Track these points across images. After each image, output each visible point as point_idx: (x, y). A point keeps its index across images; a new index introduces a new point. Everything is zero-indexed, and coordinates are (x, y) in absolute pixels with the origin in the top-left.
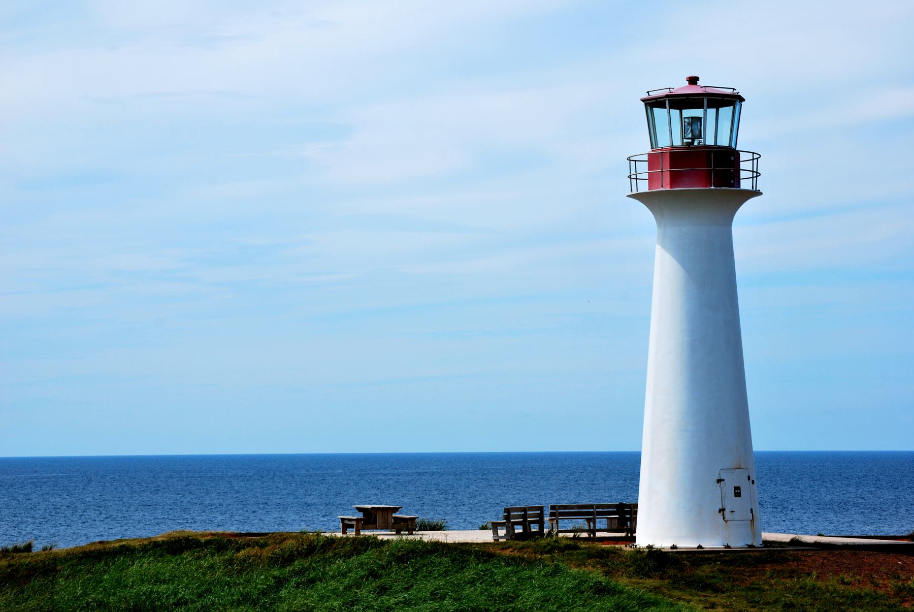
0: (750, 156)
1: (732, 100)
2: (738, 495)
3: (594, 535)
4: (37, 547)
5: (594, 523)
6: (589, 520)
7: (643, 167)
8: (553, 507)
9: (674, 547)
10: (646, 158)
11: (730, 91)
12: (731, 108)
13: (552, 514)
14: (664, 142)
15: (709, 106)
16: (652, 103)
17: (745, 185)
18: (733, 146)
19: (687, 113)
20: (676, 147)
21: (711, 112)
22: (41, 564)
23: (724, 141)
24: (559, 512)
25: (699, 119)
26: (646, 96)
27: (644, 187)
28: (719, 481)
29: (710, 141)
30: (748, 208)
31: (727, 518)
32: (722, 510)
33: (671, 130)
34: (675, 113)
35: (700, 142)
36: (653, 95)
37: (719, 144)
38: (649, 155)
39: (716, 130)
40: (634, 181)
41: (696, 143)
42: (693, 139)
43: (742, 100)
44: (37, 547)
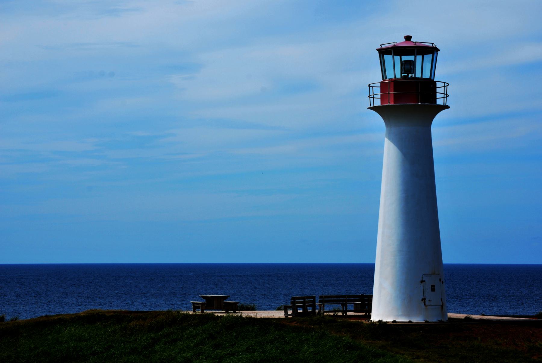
0: (442, 85)
1: (433, 50)
3: (346, 314)
6: (343, 305)
7: (378, 91)
8: (321, 297)
10: (379, 85)
13: (320, 301)
14: (390, 75)
16: (383, 52)
17: (440, 102)
18: (432, 78)
19: (405, 58)
20: (390, 82)
21: (419, 58)
27: (378, 103)
29: (418, 75)
39: (422, 69)
43: (439, 50)
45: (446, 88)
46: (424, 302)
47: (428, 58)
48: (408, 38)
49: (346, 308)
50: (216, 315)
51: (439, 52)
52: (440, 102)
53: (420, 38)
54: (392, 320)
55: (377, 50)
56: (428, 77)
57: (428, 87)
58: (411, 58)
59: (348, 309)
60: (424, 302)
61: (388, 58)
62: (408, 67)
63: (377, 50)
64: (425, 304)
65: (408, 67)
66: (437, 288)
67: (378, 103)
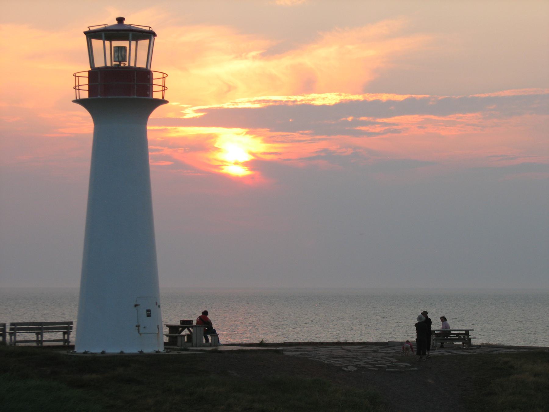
0: (161, 75)
1: (149, 35)
2: (149, 315)
3: (42, 344)
4: (218, 156)
5: (15, 336)
6: (37, 334)
7: (85, 81)
8: (12, 324)
9: (103, 352)
10: (87, 74)
11: (147, 29)
12: (148, 41)
13: (11, 329)
14: (99, 63)
15: (133, 40)
16: (91, 35)
17: (157, 95)
18: (149, 68)
19: (116, 44)
20: (105, 70)
21: (133, 43)
22: (148, 93)
23: (141, 64)
24: (16, 327)
25: (125, 48)
26: (87, 30)
27: (85, 95)
28: (136, 306)
29: (132, 65)
30: (157, 113)
31: (141, 331)
32: (138, 326)
33: (104, 53)
34: (107, 43)
35: (125, 64)
36: (91, 29)
37: (138, 66)
38: (89, 72)
39: (137, 55)
40: (77, 91)
41: (122, 65)
42: (120, 62)
43: (155, 35)
44: (218, 156)
45: (77, 85)
46: (138, 330)
47: (144, 43)
48: (120, 20)
49: (42, 337)
50: (495, 352)
51: (156, 38)
52: (157, 95)
53: (133, 20)
54: (101, 351)
55: (85, 33)
56: (144, 66)
57: (144, 77)
58: (125, 44)
59: (44, 339)
60: (138, 330)
61: (97, 44)
62: (120, 52)
63: (85, 33)
64: (139, 332)
65: (120, 52)
66: (145, 313)
67: (85, 95)
